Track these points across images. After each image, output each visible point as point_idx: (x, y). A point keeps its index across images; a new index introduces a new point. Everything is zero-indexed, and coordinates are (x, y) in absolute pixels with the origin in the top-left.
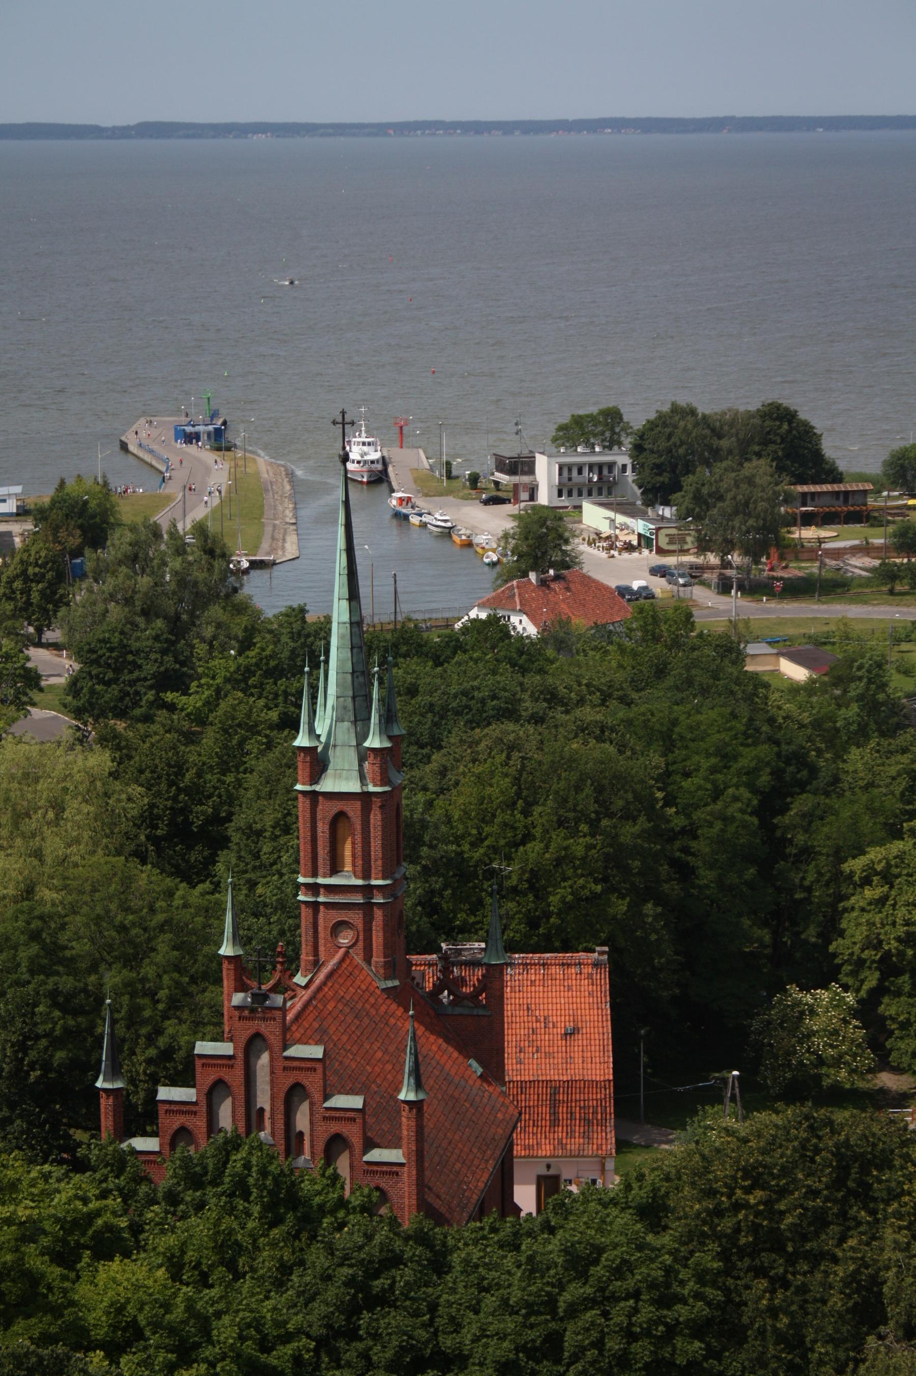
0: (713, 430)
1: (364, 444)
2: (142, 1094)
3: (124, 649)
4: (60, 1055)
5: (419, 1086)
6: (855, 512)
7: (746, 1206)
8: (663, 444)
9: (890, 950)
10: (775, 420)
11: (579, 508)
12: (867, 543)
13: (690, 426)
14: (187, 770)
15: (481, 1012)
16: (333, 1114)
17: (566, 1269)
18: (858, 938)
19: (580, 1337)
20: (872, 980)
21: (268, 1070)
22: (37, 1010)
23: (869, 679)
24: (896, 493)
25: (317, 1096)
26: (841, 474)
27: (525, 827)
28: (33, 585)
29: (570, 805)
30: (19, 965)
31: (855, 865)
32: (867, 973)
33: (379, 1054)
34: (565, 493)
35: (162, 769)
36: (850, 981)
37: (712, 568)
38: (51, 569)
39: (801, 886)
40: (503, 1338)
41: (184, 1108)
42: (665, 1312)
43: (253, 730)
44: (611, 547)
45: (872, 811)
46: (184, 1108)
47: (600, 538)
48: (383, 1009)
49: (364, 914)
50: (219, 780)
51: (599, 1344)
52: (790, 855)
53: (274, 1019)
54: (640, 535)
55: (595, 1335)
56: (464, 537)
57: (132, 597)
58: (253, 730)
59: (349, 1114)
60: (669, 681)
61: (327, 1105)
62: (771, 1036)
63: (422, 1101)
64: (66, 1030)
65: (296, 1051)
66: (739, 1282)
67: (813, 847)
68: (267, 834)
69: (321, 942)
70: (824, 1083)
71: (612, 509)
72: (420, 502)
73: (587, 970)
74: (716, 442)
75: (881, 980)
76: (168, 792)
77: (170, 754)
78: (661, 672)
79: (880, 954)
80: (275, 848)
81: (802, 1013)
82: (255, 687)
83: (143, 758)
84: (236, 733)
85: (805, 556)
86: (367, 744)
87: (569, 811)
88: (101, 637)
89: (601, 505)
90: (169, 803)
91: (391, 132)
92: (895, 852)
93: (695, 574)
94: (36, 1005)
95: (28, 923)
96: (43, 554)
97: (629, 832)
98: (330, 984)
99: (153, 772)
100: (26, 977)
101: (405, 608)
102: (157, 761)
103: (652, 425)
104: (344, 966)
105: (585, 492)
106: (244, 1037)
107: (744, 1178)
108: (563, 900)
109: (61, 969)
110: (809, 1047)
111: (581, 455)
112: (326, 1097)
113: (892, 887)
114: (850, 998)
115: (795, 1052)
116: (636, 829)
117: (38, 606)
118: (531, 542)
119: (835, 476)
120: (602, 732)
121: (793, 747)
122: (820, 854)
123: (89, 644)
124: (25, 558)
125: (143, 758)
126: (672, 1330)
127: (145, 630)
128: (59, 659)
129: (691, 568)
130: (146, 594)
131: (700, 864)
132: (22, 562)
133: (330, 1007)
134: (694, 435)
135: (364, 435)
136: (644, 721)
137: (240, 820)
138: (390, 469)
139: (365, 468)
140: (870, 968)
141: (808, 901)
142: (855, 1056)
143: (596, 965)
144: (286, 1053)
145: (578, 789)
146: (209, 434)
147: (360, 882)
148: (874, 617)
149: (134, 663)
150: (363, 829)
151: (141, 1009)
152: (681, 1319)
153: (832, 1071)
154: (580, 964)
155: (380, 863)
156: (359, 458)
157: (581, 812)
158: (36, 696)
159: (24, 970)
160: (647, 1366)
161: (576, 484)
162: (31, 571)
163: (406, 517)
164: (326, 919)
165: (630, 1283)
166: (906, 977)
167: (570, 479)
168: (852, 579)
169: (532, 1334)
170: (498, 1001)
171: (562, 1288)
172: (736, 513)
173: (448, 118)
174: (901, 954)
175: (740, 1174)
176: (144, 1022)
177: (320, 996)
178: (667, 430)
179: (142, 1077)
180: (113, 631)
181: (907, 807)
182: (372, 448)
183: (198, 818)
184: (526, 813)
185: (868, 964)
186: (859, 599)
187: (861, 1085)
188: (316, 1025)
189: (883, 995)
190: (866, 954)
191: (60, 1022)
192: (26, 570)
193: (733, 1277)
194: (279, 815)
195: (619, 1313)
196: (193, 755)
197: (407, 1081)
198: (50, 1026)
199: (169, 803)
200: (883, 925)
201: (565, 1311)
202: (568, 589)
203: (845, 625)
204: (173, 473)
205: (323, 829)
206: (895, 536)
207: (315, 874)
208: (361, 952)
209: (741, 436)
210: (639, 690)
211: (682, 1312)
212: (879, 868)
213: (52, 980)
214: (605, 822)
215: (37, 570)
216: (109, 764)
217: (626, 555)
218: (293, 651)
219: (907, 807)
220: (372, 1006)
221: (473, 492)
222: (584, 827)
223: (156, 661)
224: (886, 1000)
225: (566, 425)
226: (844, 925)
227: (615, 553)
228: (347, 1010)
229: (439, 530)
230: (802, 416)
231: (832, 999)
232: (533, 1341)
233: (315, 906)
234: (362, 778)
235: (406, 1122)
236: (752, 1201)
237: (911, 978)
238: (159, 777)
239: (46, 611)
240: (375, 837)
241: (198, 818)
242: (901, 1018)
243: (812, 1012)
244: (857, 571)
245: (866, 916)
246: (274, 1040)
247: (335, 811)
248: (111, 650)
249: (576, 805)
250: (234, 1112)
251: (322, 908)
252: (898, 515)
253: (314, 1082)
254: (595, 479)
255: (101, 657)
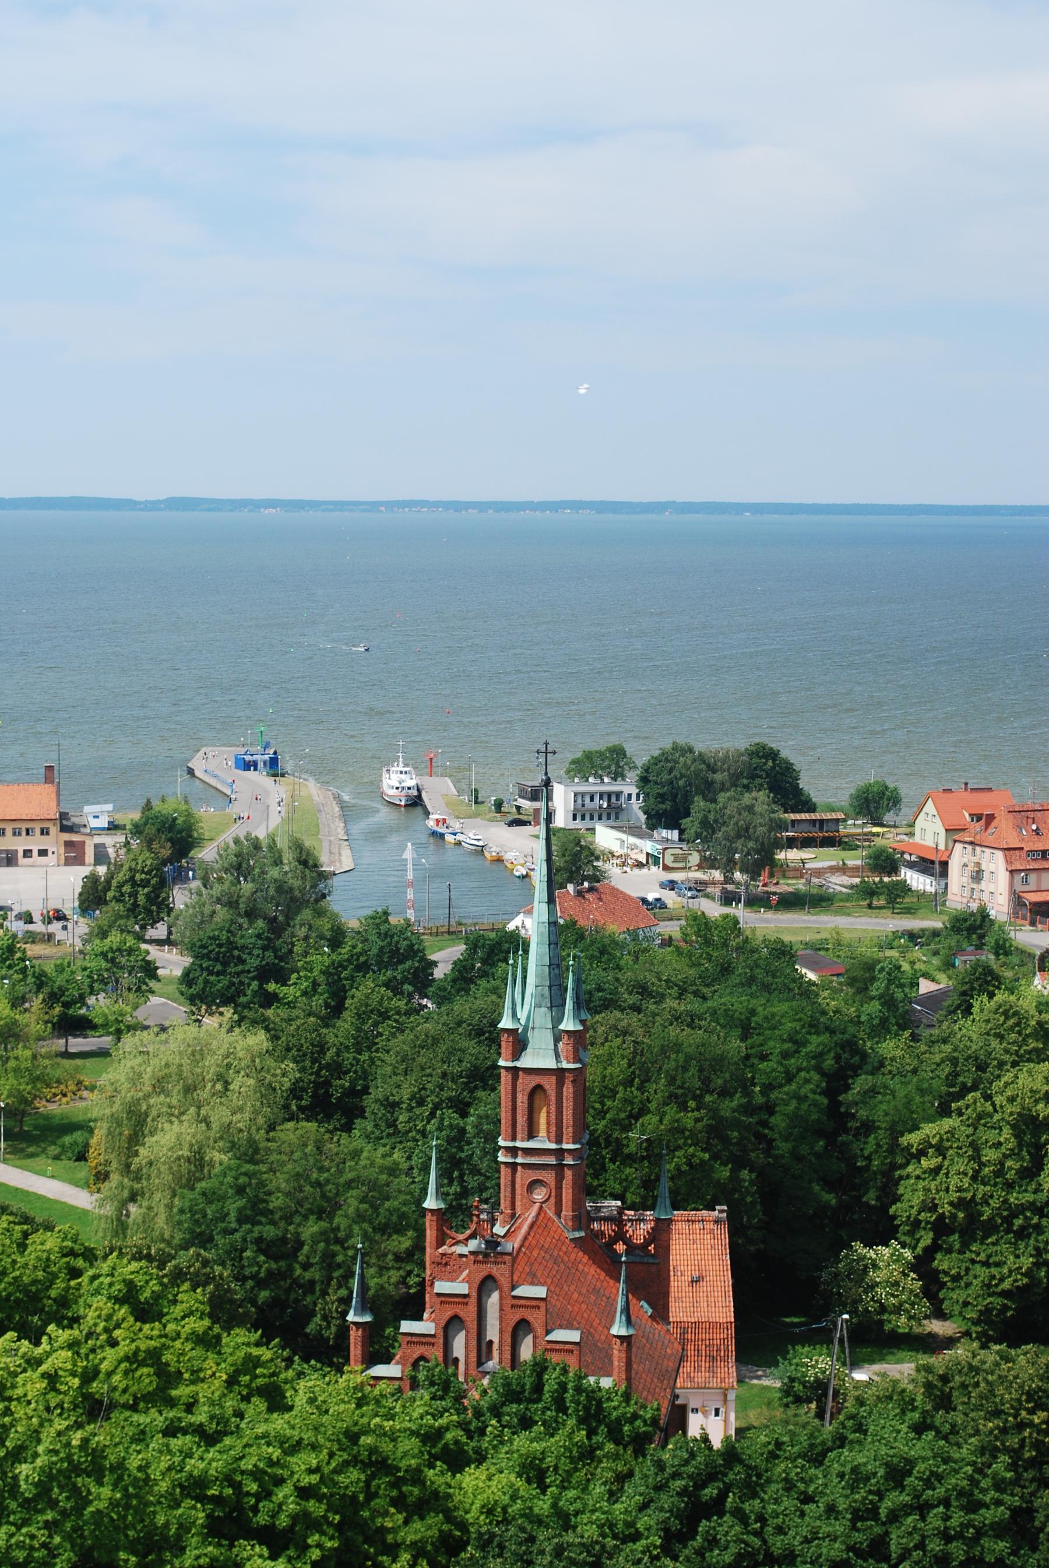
0: (708, 766)
1: (401, 772)
2: (333, 1329)
3: (231, 945)
4: (264, 1295)
5: (629, 1322)
6: (829, 837)
7: (1031, 1424)
8: (665, 777)
9: (944, 1213)
10: (760, 758)
11: (592, 830)
12: (844, 864)
13: (689, 762)
14: (328, 1050)
15: (651, 1260)
16: (554, 1346)
17: (886, 1479)
18: (916, 1201)
19: (904, 1540)
20: (926, 1239)
21: (497, 1307)
22: (244, 1254)
23: (889, 980)
24: (860, 822)
25: (540, 1331)
26: (815, 805)
27: (641, 1102)
28: (140, 889)
29: (679, 1082)
30: (227, 1214)
31: (913, 1139)
32: (923, 1233)
33: (575, 1295)
34: (579, 817)
35: (307, 1048)
36: (908, 1240)
37: (714, 883)
38: (155, 876)
39: (862, 1156)
40: (835, 1540)
41: (423, 1340)
42: (972, 1516)
43: (384, 1016)
44: (623, 864)
45: (922, 1092)
46: (423, 1340)
47: (613, 856)
48: (573, 1256)
49: (556, 1174)
50: (354, 1058)
51: (921, 1546)
52: (851, 1128)
53: (505, 1263)
54: (648, 854)
55: (917, 1537)
56: (494, 854)
57: (237, 901)
58: (384, 1016)
59: (567, 1347)
60: (735, 979)
61: (548, 1338)
62: (840, 1287)
63: (631, 1336)
64: (269, 1272)
65: (523, 1291)
66: (1025, 1491)
67: (874, 1121)
68: (404, 1106)
69: (518, 1197)
70: (886, 1328)
71: (625, 832)
72: (456, 825)
73: (709, 1226)
74: (710, 776)
75: (934, 1240)
76: (311, 1068)
77: (314, 1036)
78: (726, 970)
79: (934, 1217)
80: (410, 1118)
81: (866, 1267)
82: (347, 979)
83: (290, 1038)
84: (369, 1018)
85: (791, 874)
86: (562, 1027)
87: (679, 1087)
88: (211, 934)
89: (612, 827)
90: (313, 1078)
91: (383, 509)
92: (947, 1128)
93: (699, 888)
94: (243, 1250)
95: (236, 1179)
96: (148, 863)
97: (729, 1107)
98: (532, 1234)
99: (298, 1050)
100: (234, 1225)
101: (457, 914)
102: (303, 1041)
103: (656, 761)
104: (541, 1218)
105: (596, 817)
106: (478, 1279)
107: (1027, 1401)
108: (678, 1168)
109: (263, 1220)
110: (873, 1297)
111: (593, 785)
112: (548, 1332)
113: (944, 1158)
114: (908, 1254)
115: (862, 1300)
116: (735, 1104)
117: (144, 908)
118: (567, 858)
119: (812, 808)
120: (693, 1020)
121: (847, 1036)
122: (879, 1128)
123: (201, 940)
124: (133, 866)
125: (290, 1038)
126: (980, 1533)
127: (248, 929)
128: (161, 954)
129: (696, 883)
130: (248, 898)
131: (777, 1136)
132: (130, 869)
133: (535, 1254)
134: (692, 769)
135: (401, 764)
136: (725, 1010)
137: (377, 1092)
138: (424, 795)
139: (404, 793)
140: (925, 1229)
141: (867, 1168)
142: (913, 1304)
143: (717, 1221)
144: (514, 1293)
145: (685, 1069)
146: (265, 763)
147: (553, 1146)
148: (858, 927)
149: (239, 958)
150: (557, 1100)
151: (334, 1255)
152: (987, 1522)
153: (893, 1317)
154: (703, 1221)
155: (571, 1129)
156: (398, 785)
157: (688, 1089)
158: (152, 984)
159: (233, 1219)
160: (961, 1563)
161: (589, 810)
162: (138, 877)
163: (442, 836)
164: (523, 1178)
165: (940, 1491)
166: (956, 1236)
167: (583, 805)
168: (834, 895)
169: (858, 1537)
170: (664, 1251)
171: (880, 1495)
172: (739, 836)
173: (432, 498)
174: (953, 1216)
175: (1024, 1398)
176: (339, 1266)
177: (527, 1244)
178: (669, 765)
179: (334, 1315)
180: (221, 929)
181: (951, 1090)
182: (408, 776)
183: (337, 1091)
184: (641, 1089)
185: (923, 1224)
186: (842, 912)
187: (917, 1330)
188: (527, 1269)
189: (936, 1252)
190: (923, 1216)
191: (267, 1266)
192: (134, 876)
193: (1020, 1486)
194: (416, 1090)
195: (934, 1519)
196: (330, 1036)
197: (619, 1318)
198: (256, 1269)
199: (313, 1078)
200: (938, 1191)
201: (887, 1517)
202: (600, 899)
203: (837, 933)
204: (238, 795)
205: (522, 1099)
206: (870, 857)
207: (514, 1139)
208: (553, 1207)
209: (732, 772)
210: (707, 985)
211: (989, 1515)
212: (934, 1142)
213: (257, 1228)
214: (708, 1098)
215: (143, 876)
216: (265, 1044)
217: (636, 871)
218: (381, 948)
219: (951, 1090)
220: (565, 1253)
221: (498, 815)
222: (692, 1104)
223: (258, 956)
224: (939, 1256)
225: (578, 759)
226: (901, 1191)
227: (628, 869)
228: (547, 1257)
229: (473, 848)
230: (784, 754)
231: (892, 1255)
232: (861, 1543)
233: (514, 1166)
234: (557, 1056)
235: (618, 1353)
236: (1037, 1421)
237: (960, 1237)
238: (304, 1055)
239: (150, 911)
240: (567, 1107)
241: (337, 1091)
242: (953, 1272)
243: (875, 1266)
244: (839, 888)
245: (921, 1184)
246: (504, 1281)
247: (533, 1084)
248: (220, 946)
249: (684, 1083)
250: (467, 1344)
251: (519, 1168)
252: (865, 840)
253: (537, 1319)
254: (605, 806)
255: (211, 952)
